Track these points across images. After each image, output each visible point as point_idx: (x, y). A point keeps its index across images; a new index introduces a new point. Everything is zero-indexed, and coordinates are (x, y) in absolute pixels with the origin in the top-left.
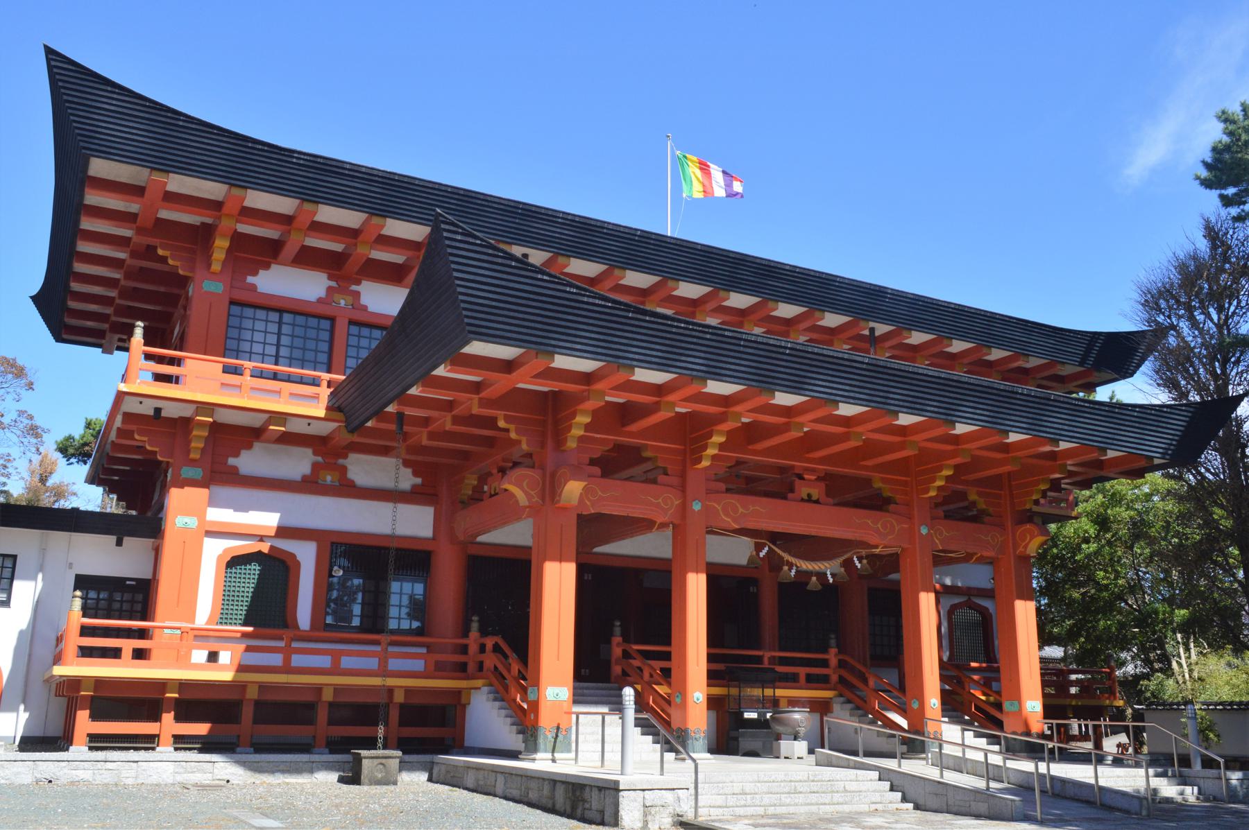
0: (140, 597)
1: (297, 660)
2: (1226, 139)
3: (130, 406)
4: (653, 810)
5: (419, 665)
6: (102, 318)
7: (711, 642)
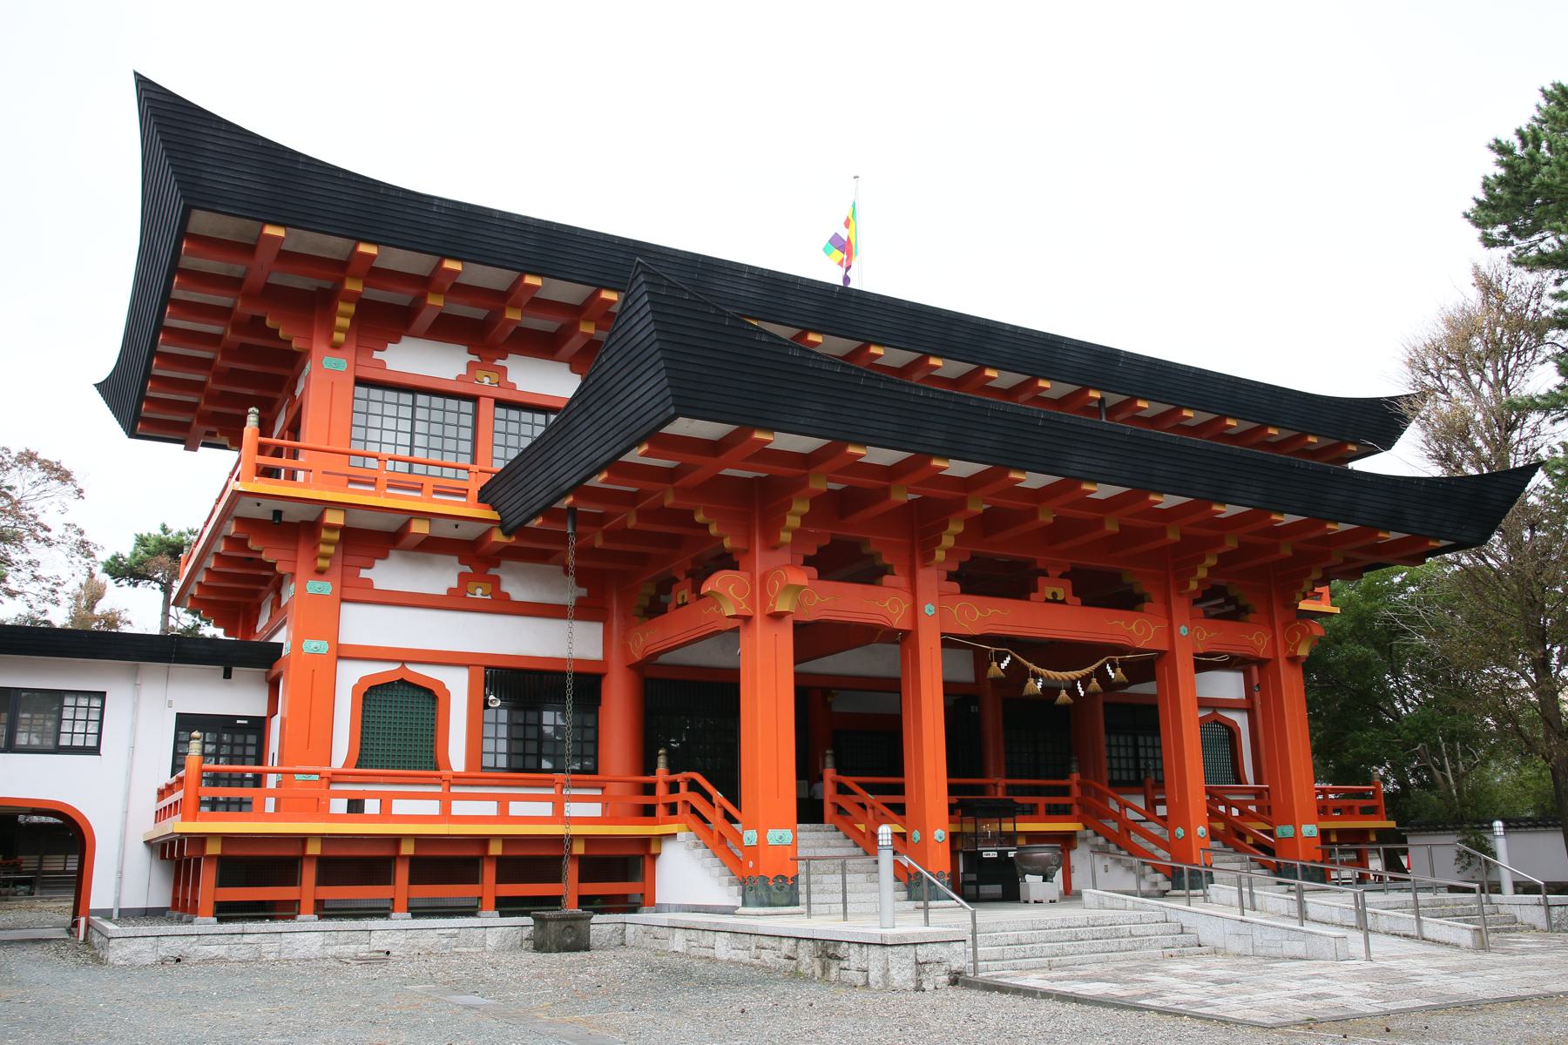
0: (252, 739)
1: (458, 808)
2: (1501, 172)
3: (247, 509)
4: (927, 967)
5: (595, 809)
6: (190, 407)
7: (952, 771)
